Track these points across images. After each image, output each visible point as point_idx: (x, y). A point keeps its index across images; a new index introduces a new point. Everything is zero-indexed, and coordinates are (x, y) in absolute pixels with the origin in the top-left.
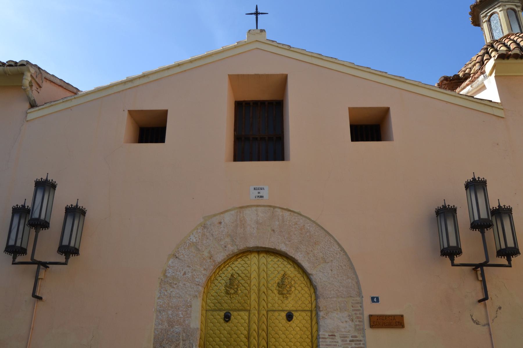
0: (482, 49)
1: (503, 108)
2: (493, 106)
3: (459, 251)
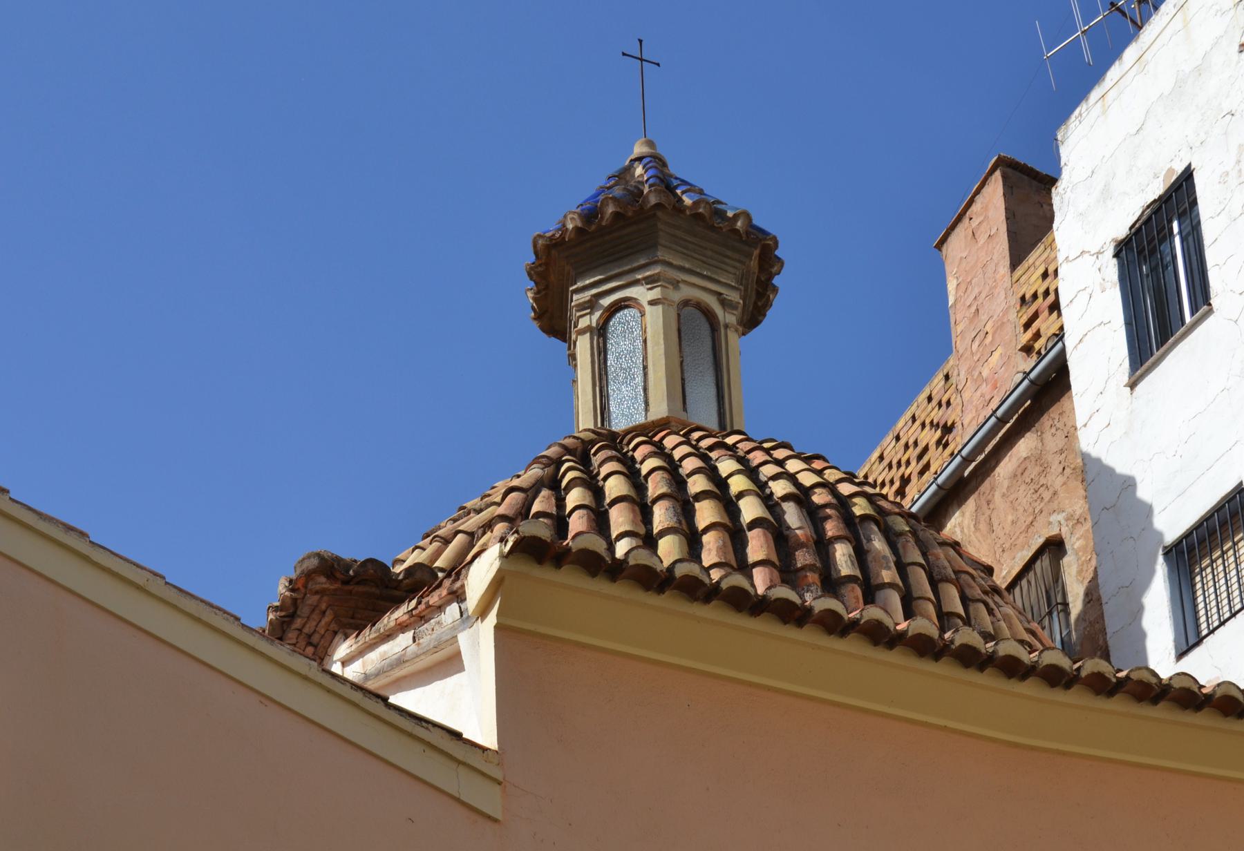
0: (537, 460)
1: (500, 777)
2: (461, 758)
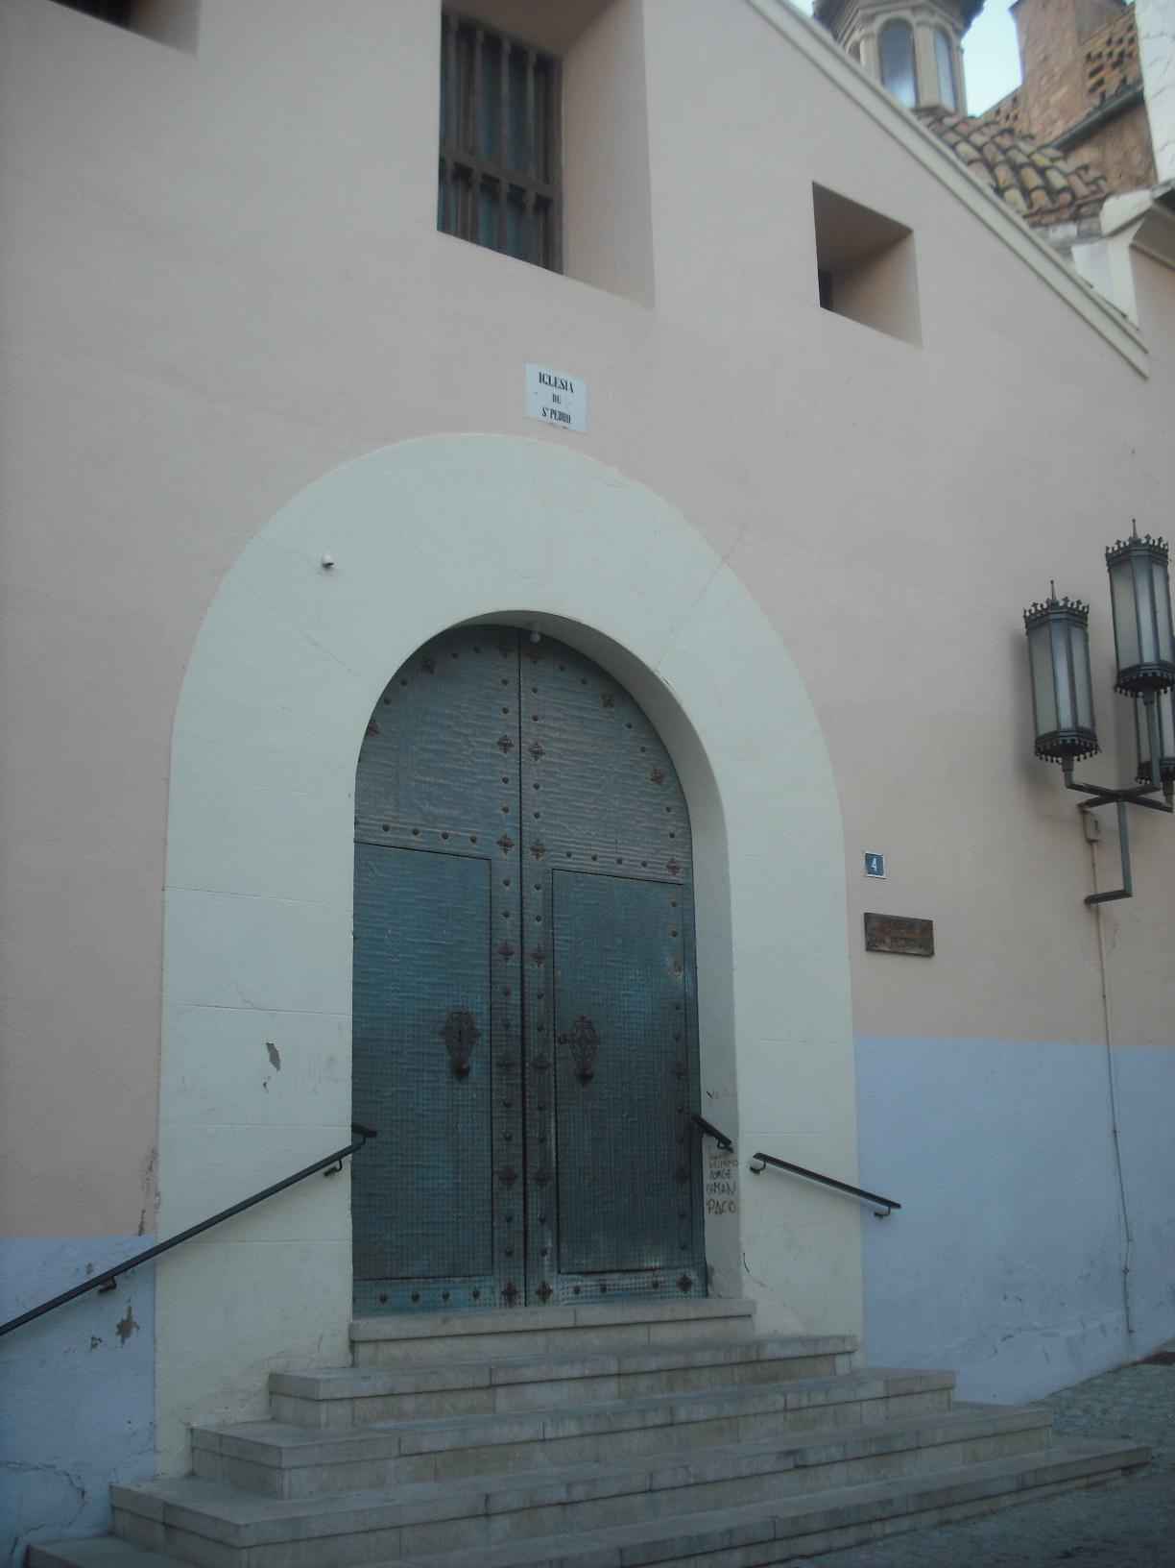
3: (1091, 745)
